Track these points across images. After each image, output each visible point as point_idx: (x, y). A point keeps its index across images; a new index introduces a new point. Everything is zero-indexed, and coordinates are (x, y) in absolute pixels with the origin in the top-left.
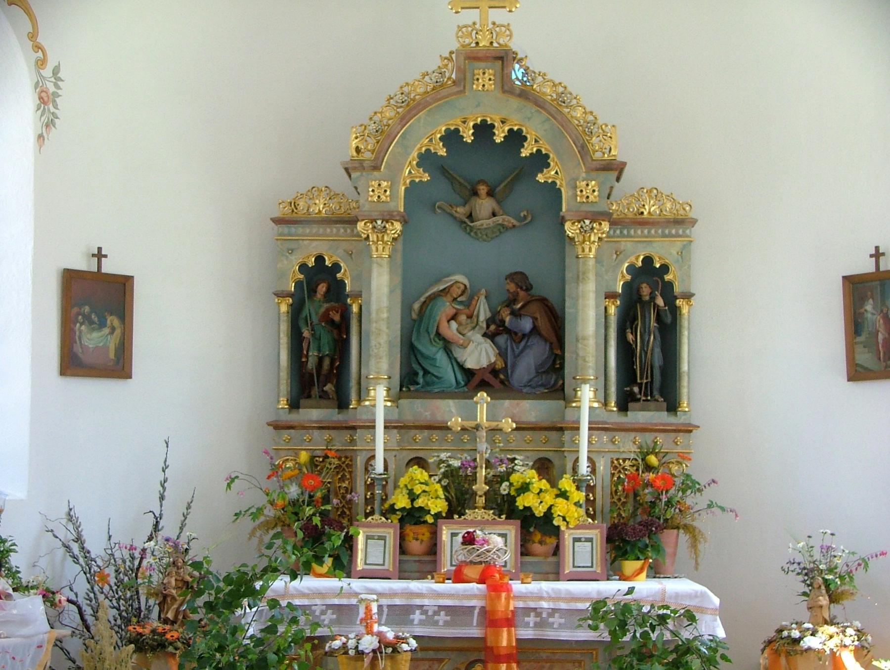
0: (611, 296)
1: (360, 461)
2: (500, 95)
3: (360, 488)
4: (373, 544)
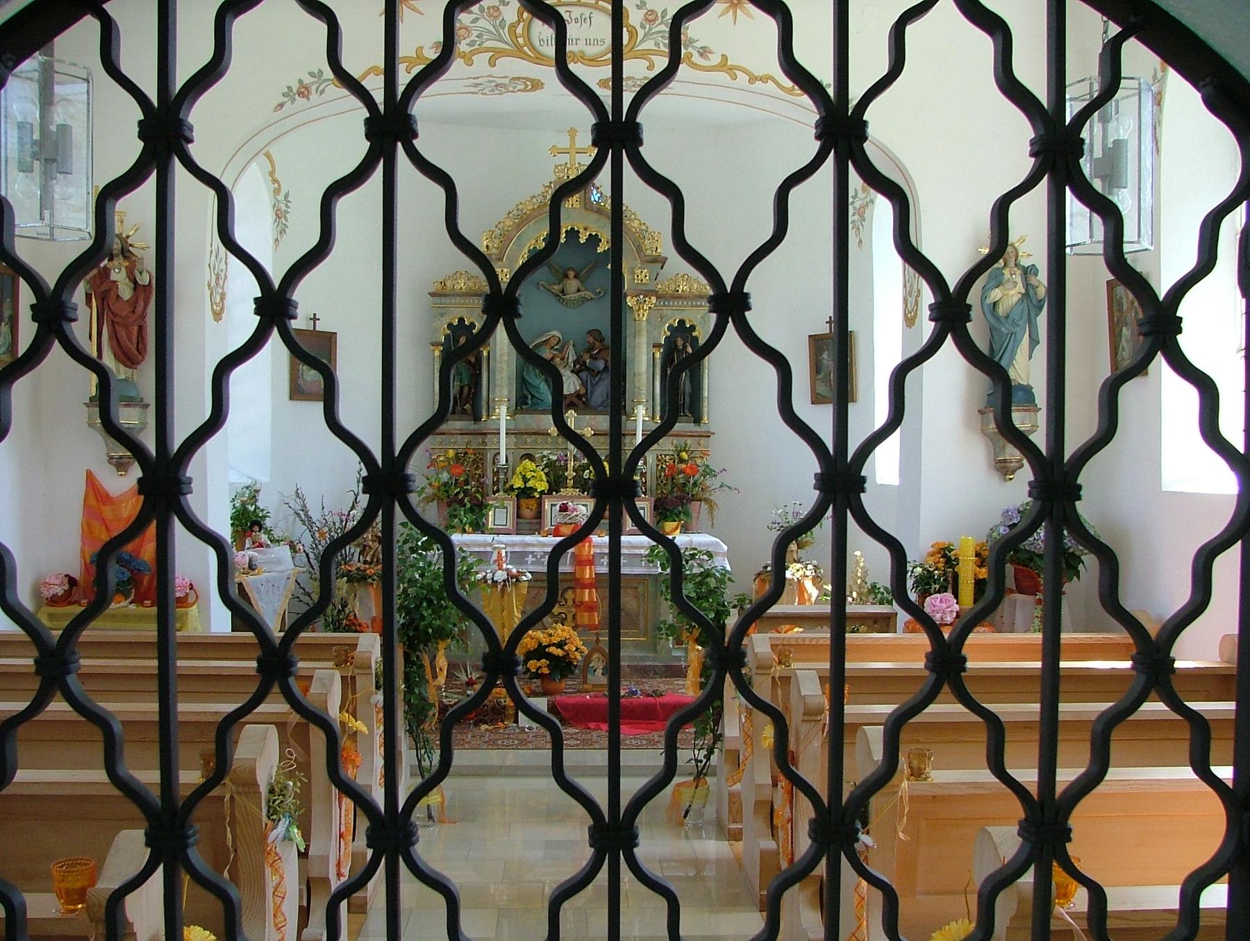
1: (489, 456)
2: (583, 211)
3: (490, 473)
4: (499, 514)
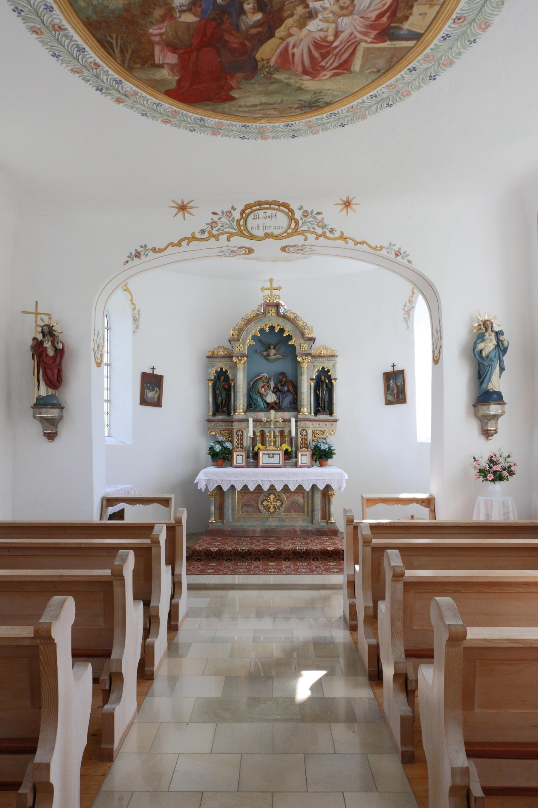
0: (312, 379)
